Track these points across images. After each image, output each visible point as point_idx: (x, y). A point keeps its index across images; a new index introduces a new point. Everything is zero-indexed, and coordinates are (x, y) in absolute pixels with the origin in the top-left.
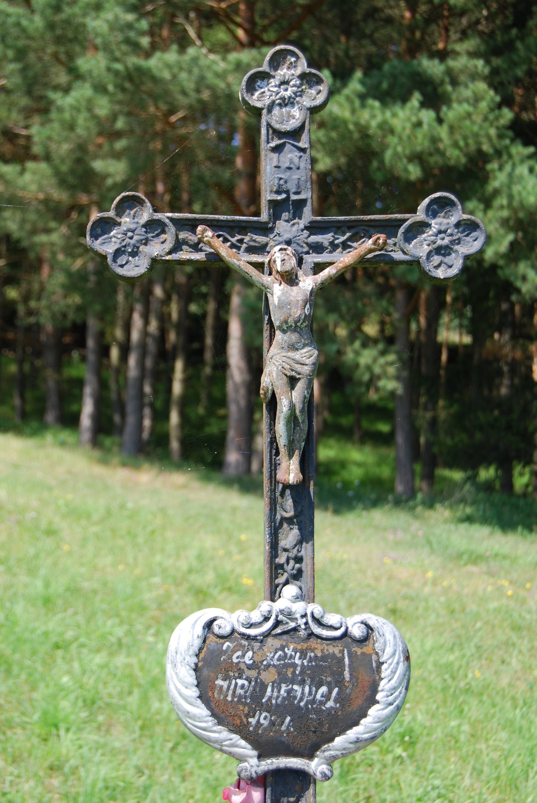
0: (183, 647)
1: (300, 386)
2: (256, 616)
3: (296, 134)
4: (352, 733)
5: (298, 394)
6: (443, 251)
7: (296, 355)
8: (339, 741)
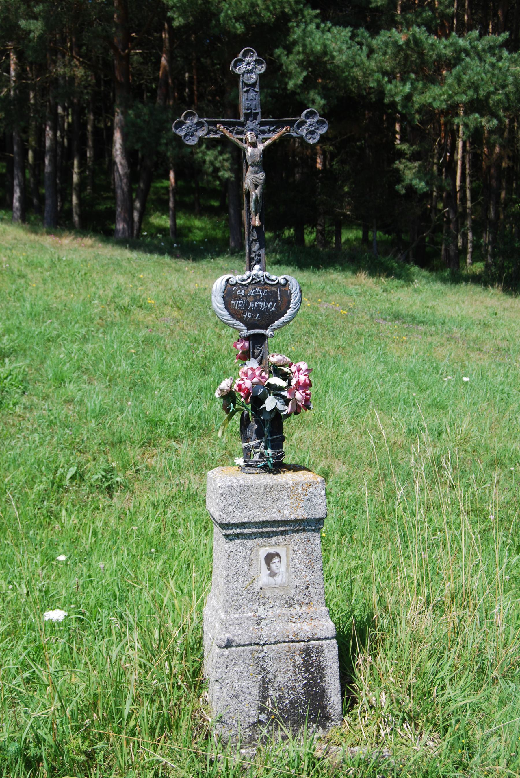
0: (218, 288)
1: (259, 187)
2: (245, 277)
3: (253, 85)
4: (282, 320)
5: (258, 191)
6: (312, 132)
7: (258, 176)
8: (276, 323)
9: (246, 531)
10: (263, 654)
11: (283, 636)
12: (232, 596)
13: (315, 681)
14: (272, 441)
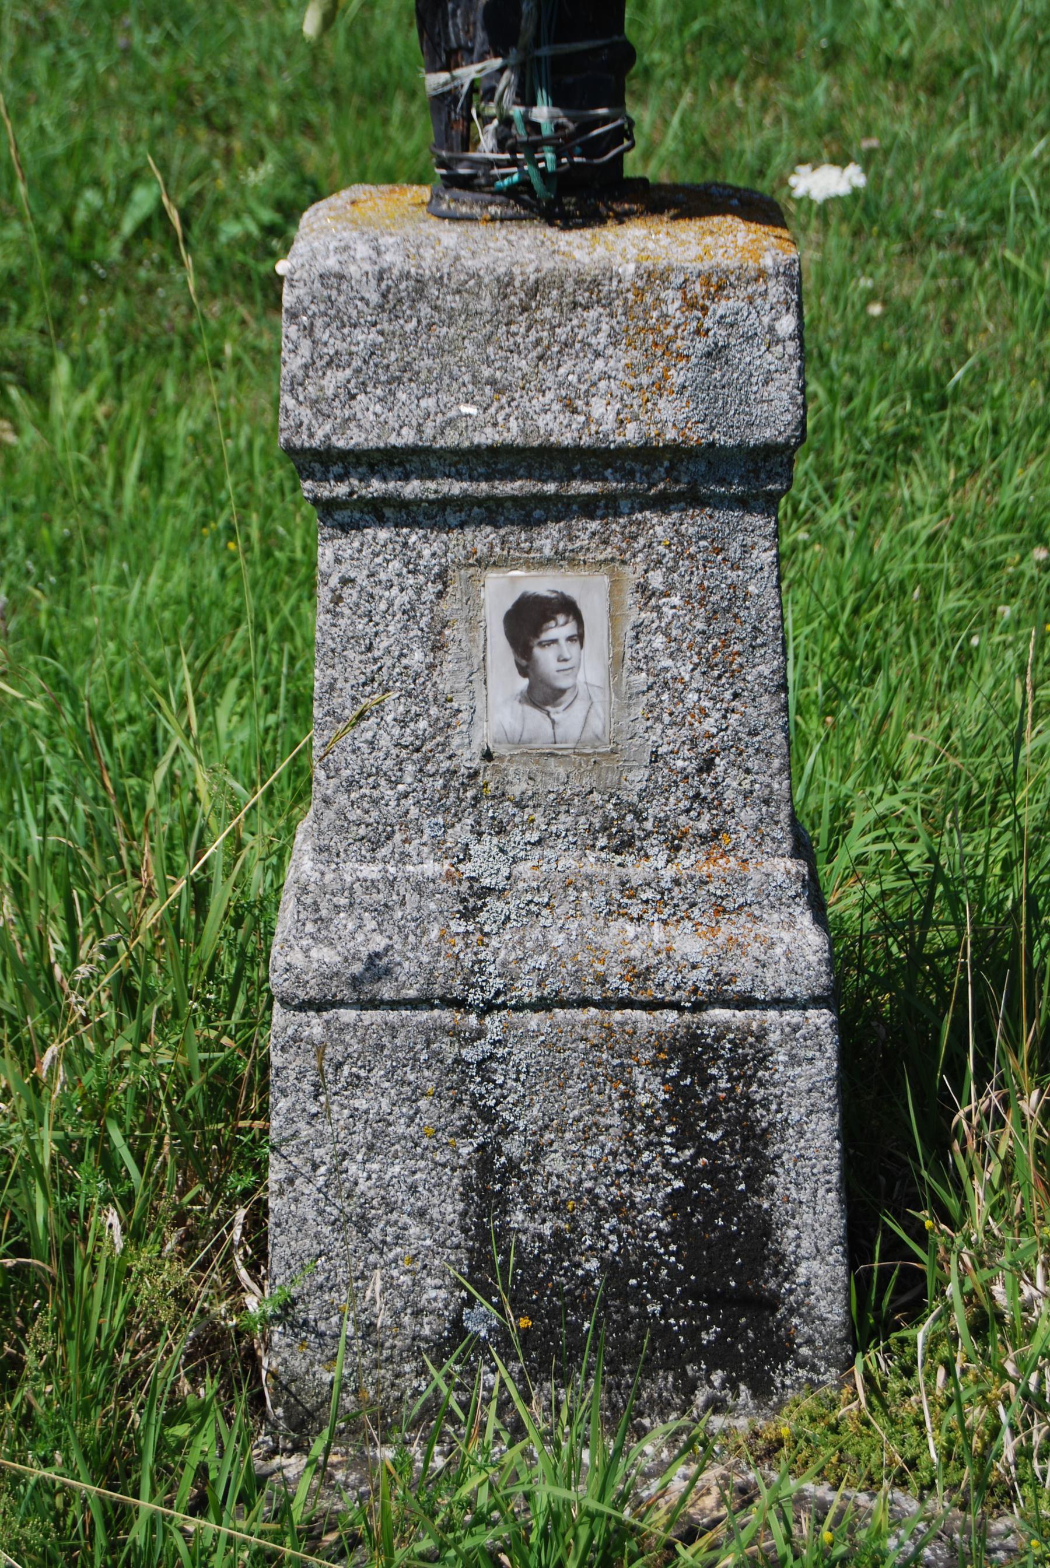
9: (412, 488)
10: (483, 1046)
11: (576, 976)
12: (351, 784)
13: (726, 1187)
14: (559, 64)
